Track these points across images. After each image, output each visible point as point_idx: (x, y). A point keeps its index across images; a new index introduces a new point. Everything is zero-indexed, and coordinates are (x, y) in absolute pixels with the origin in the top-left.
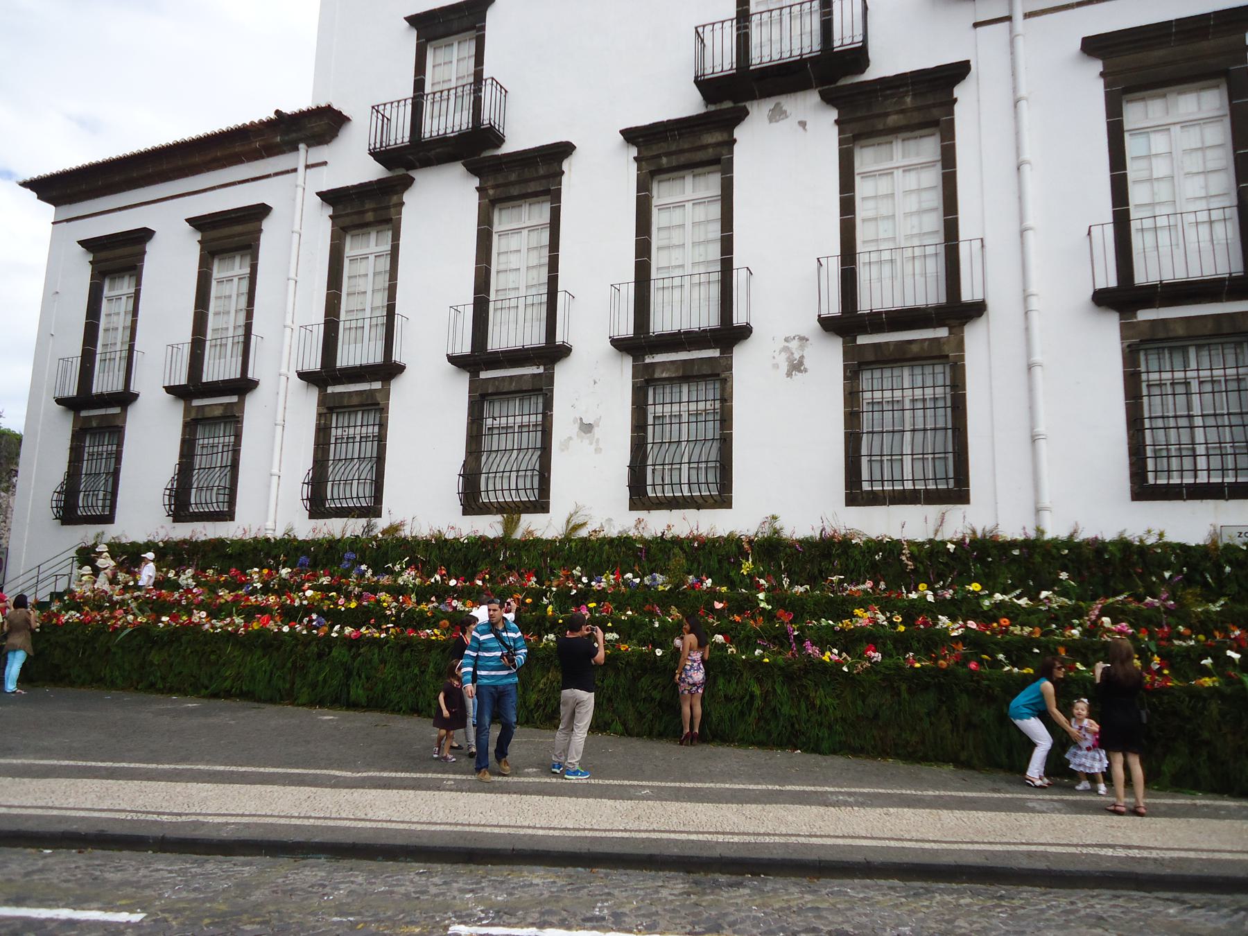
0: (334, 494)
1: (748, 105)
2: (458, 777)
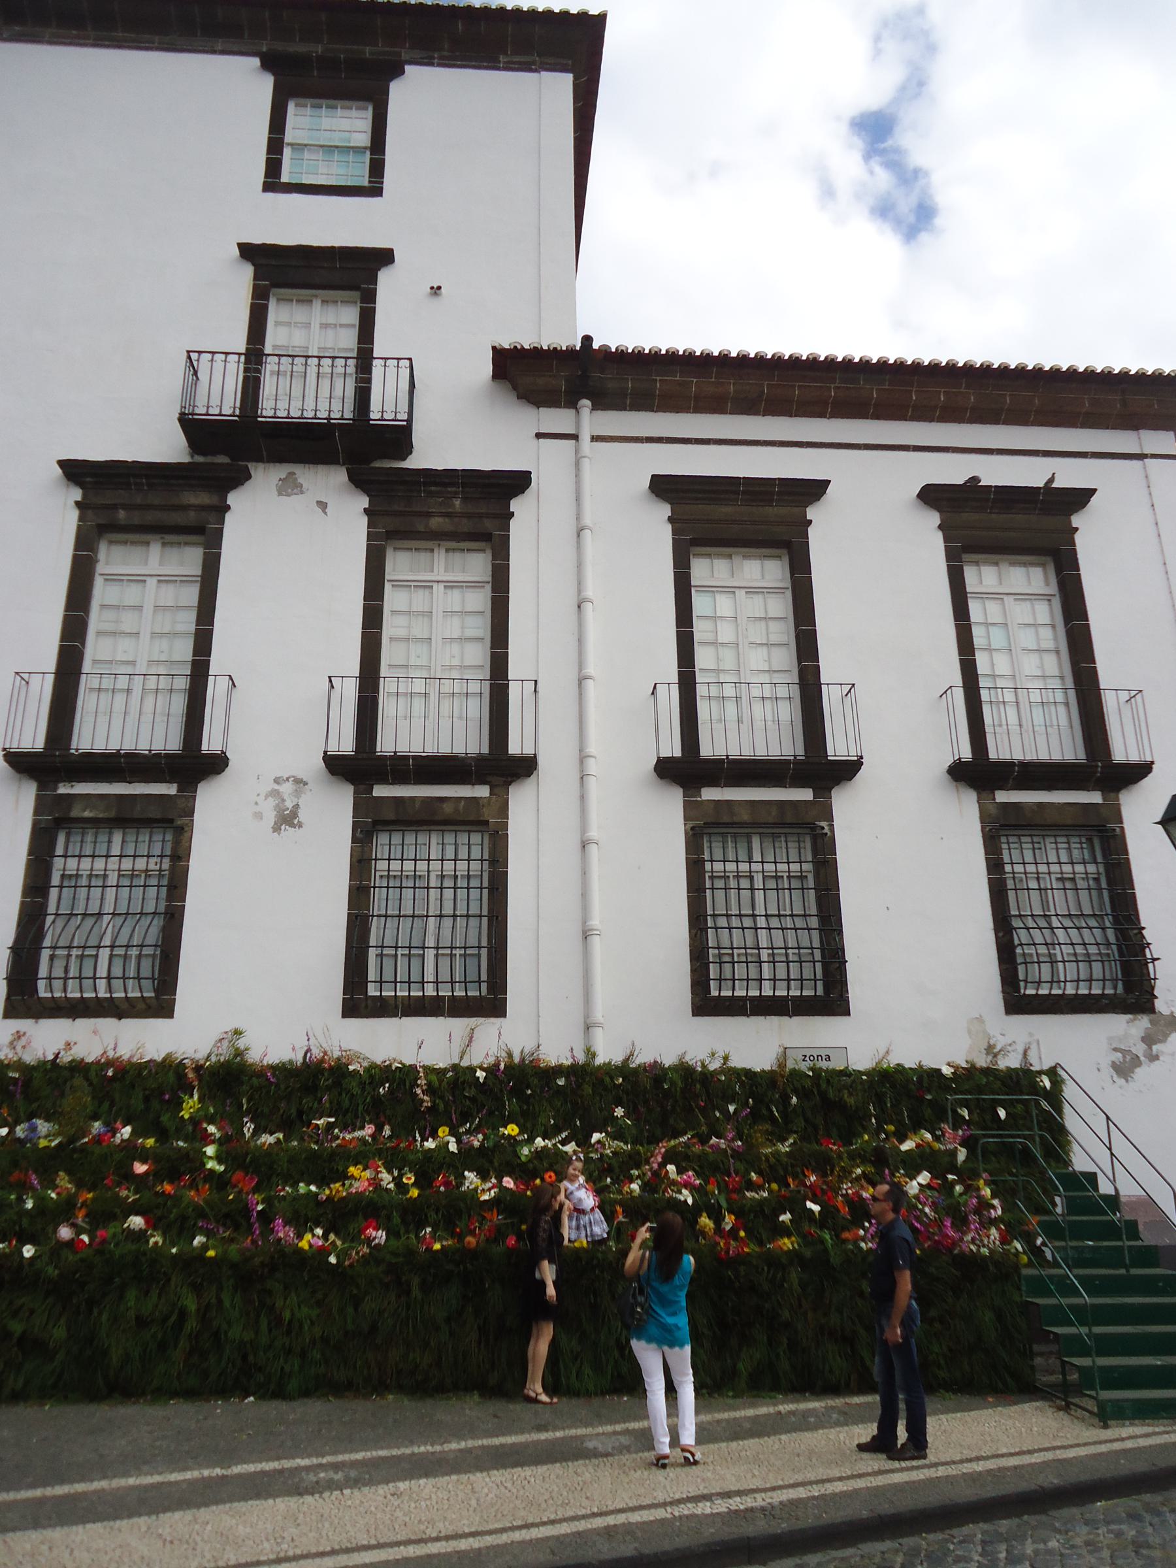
1: (251, 466)
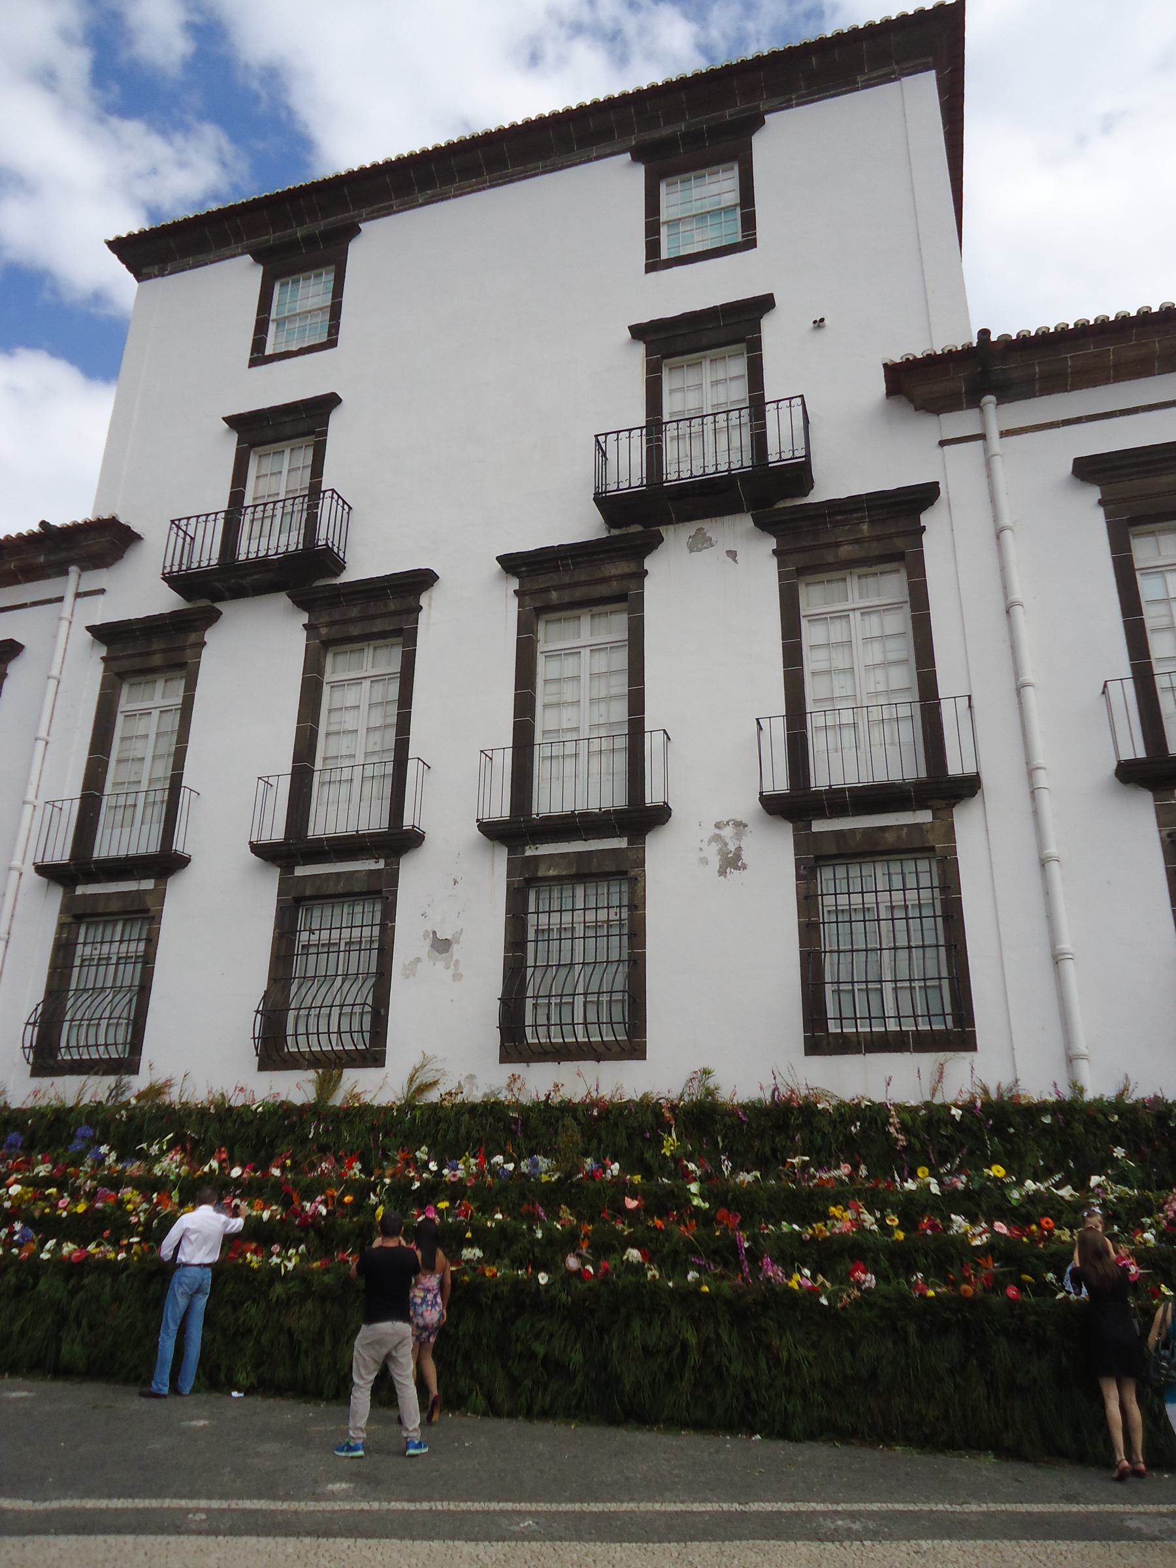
0: (73, 1041)
1: (662, 529)
2: (215, 1504)
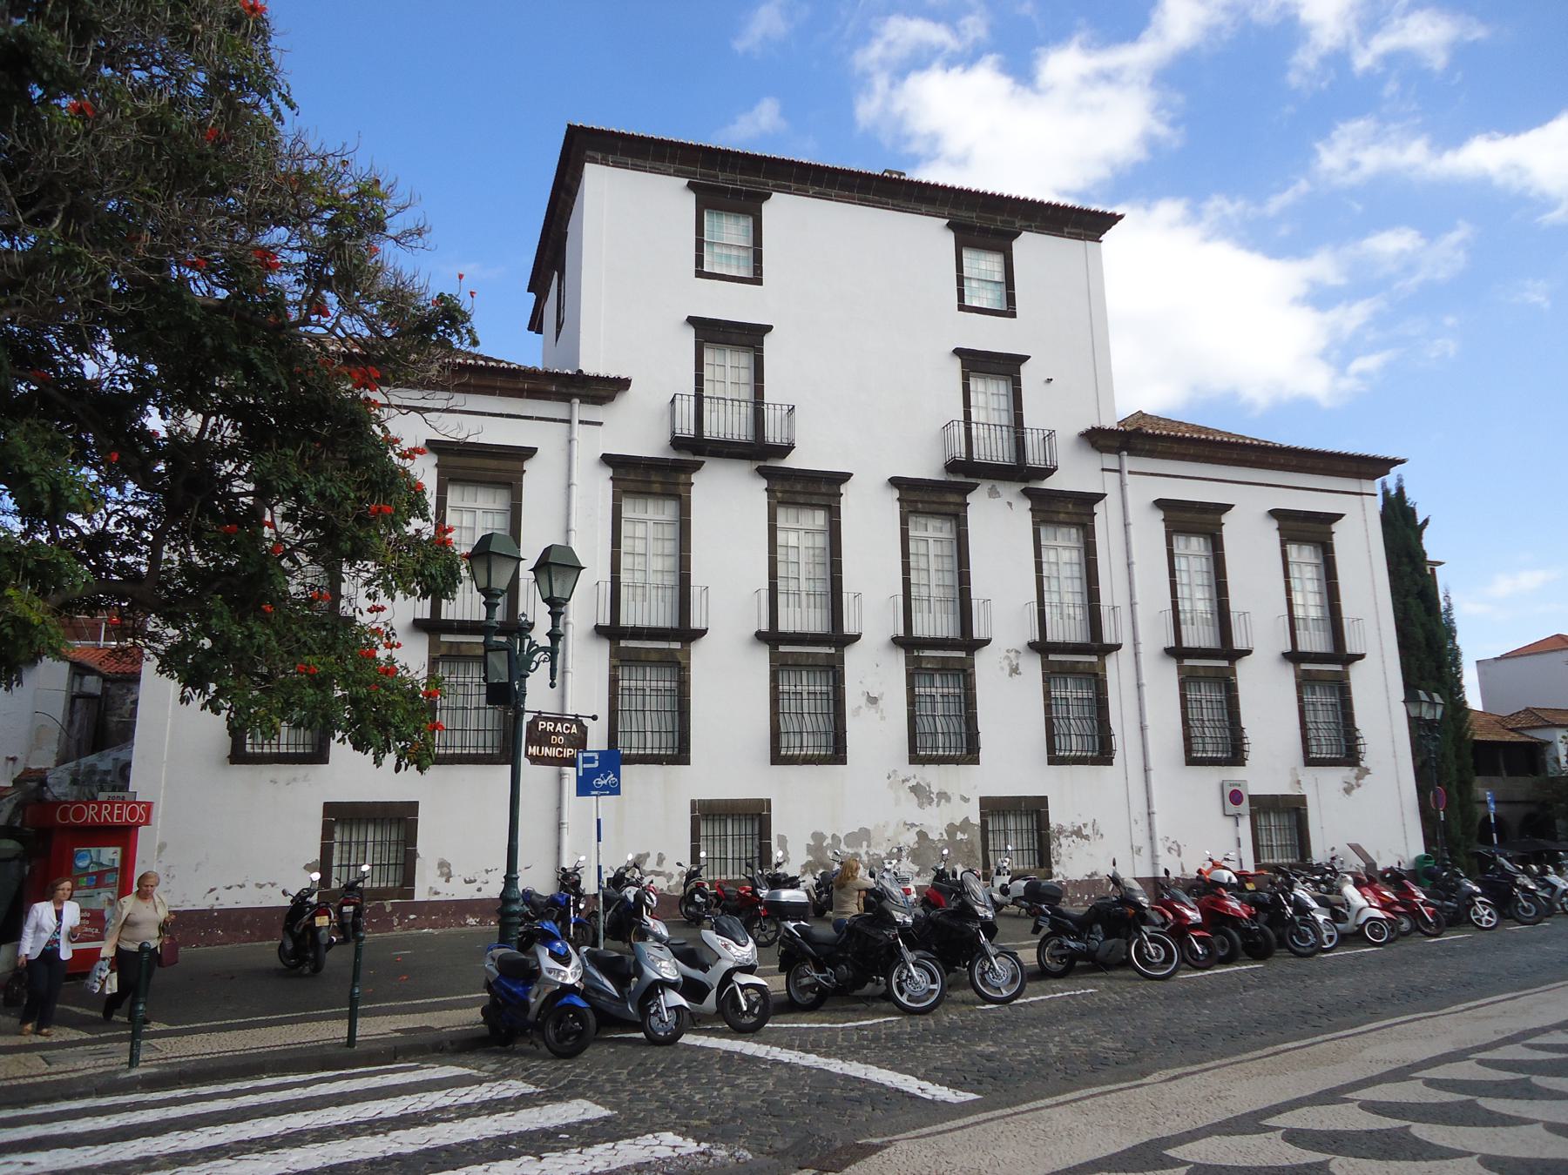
0: (790, 746)
